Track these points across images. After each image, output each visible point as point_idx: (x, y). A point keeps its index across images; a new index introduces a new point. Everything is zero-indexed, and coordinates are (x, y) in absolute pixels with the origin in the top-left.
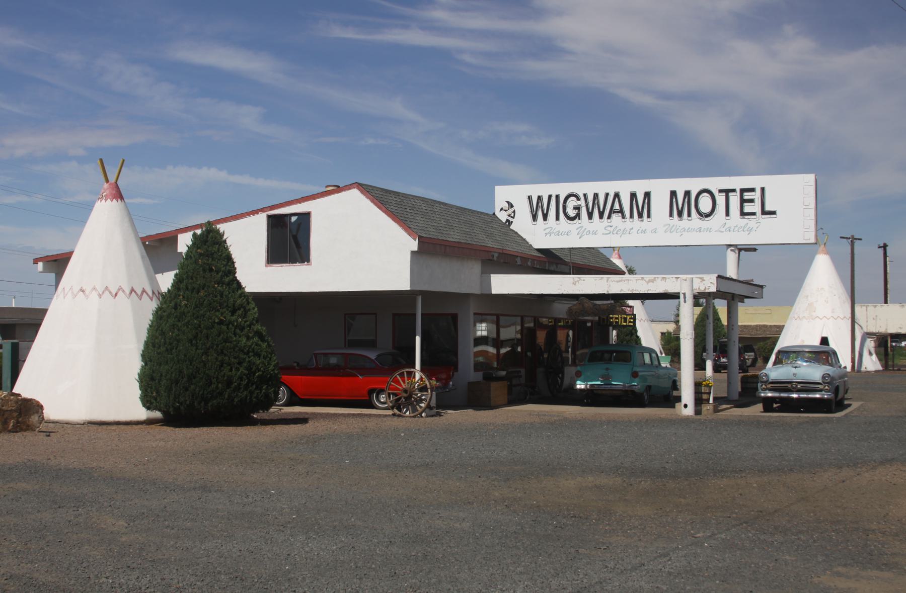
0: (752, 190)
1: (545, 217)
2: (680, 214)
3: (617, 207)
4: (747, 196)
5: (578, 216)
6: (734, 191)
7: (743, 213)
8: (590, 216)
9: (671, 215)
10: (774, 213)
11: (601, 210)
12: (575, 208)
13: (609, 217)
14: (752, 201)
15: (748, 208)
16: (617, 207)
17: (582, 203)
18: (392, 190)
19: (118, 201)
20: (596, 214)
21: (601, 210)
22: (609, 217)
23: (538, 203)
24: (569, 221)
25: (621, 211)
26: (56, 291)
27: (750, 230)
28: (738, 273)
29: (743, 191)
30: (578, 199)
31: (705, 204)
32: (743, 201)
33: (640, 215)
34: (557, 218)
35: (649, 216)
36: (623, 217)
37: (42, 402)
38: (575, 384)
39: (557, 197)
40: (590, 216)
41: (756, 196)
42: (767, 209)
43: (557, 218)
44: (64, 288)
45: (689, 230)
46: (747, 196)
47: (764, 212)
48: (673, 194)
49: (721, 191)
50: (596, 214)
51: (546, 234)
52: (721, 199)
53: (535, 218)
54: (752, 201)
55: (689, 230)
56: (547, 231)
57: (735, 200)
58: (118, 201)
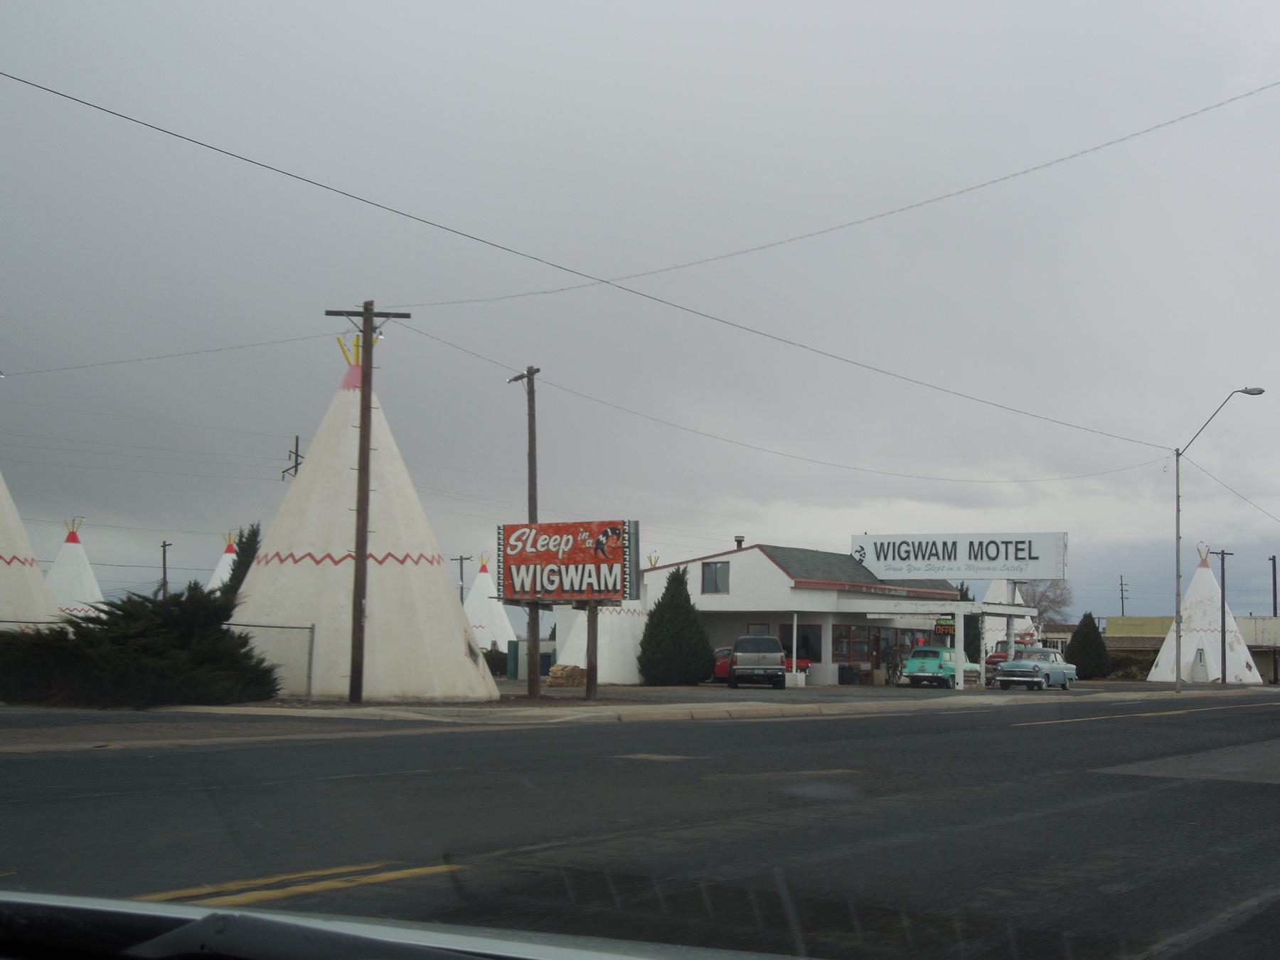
0: (1023, 542)
1: (886, 558)
2: (976, 558)
3: (934, 551)
4: (1020, 546)
5: (908, 557)
6: (1011, 542)
7: (1017, 558)
8: (916, 558)
9: (970, 558)
10: (1036, 558)
12: (906, 552)
13: (929, 559)
14: (1022, 550)
15: (1021, 554)
16: (934, 551)
17: (911, 548)
22: (929, 559)
25: (937, 555)
27: (1021, 570)
29: (1017, 543)
30: (908, 545)
31: (992, 551)
32: (1017, 550)
33: (949, 558)
34: (894, 559)
35: (955, 558)
36: (938, 559)
39: (894, 544)
40: (916, 558)
41: (1025, 546)
42: (1033, 555)
43: (894, 559)
45: (982, 569)
46: (1020, 546)
47: (1031, 558)
49: (1003, 542)
52: (1002, 547)
53: (878, 558)
54: (1022, 550)
55: (982, 569)
57: (1012, 548)
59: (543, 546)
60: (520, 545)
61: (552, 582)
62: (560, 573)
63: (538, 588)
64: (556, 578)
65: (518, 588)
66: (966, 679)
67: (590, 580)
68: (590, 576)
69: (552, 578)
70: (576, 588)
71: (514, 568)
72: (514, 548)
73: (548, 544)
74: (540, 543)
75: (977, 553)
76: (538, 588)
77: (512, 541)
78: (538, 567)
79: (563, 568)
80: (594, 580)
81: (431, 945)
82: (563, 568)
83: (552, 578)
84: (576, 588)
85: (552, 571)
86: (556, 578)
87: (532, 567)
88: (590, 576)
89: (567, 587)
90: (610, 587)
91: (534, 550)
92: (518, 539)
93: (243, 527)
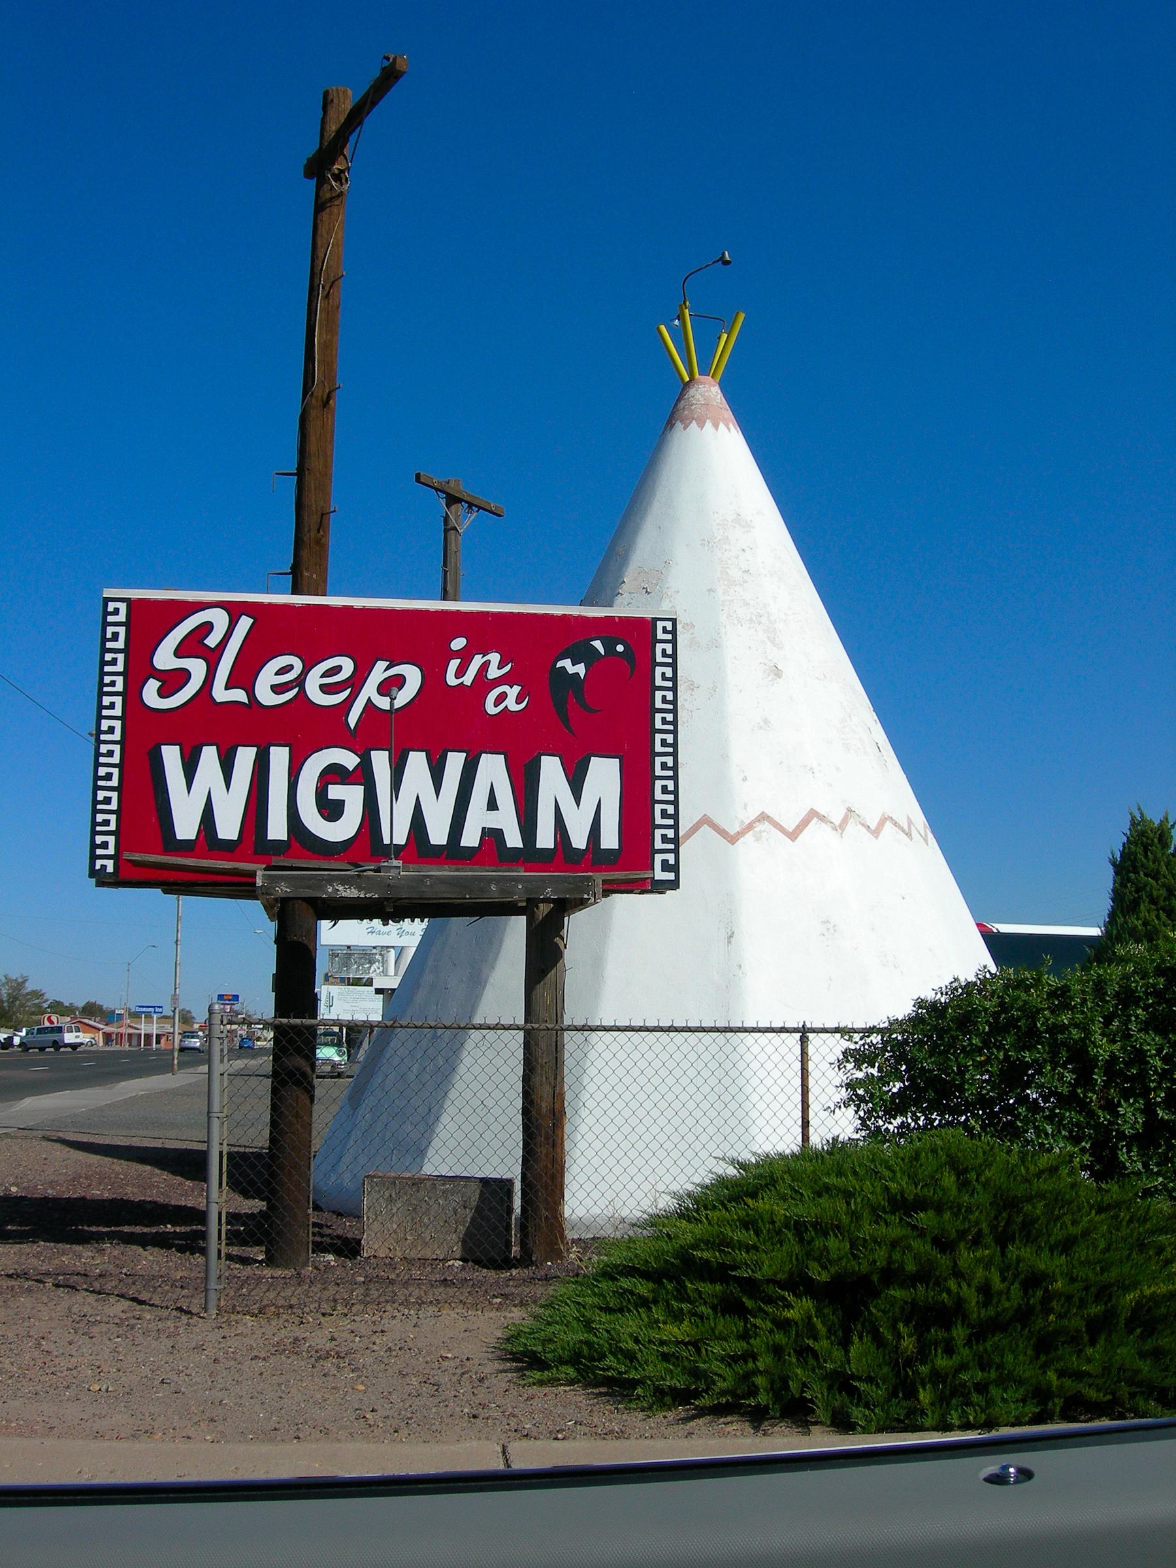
56: (370, 930)
59: (277, 689)
60: (197, 667)
61: (331, 810)
62: (363, 776)
63: (277, 829)
64: (351, 796)
65: (186, 827)
66: (250, 880)
67: (493, 820)
68: (492, 805)
69: (335, 792)
70: (438, 835)
71: (171, 756)
72: (179, 678)
73: (300, 681)
74: (267, 677)
75: (926, 835)
76: (277, 829)
77: (165, 658)
78: (279, 757)
79: (380, 761)
80: (507, 821)
81: (88, 869)
82: (380, 761)
83: (335, 792)
84: (438, 835)
85: (333, 774)
86: (351, 796)
87: (245, 757)
88: (492, 805)
89: (396, 830)
90: (579, 841)
91: (239, 695)
92: (192, 646)
93: (837, 1082)
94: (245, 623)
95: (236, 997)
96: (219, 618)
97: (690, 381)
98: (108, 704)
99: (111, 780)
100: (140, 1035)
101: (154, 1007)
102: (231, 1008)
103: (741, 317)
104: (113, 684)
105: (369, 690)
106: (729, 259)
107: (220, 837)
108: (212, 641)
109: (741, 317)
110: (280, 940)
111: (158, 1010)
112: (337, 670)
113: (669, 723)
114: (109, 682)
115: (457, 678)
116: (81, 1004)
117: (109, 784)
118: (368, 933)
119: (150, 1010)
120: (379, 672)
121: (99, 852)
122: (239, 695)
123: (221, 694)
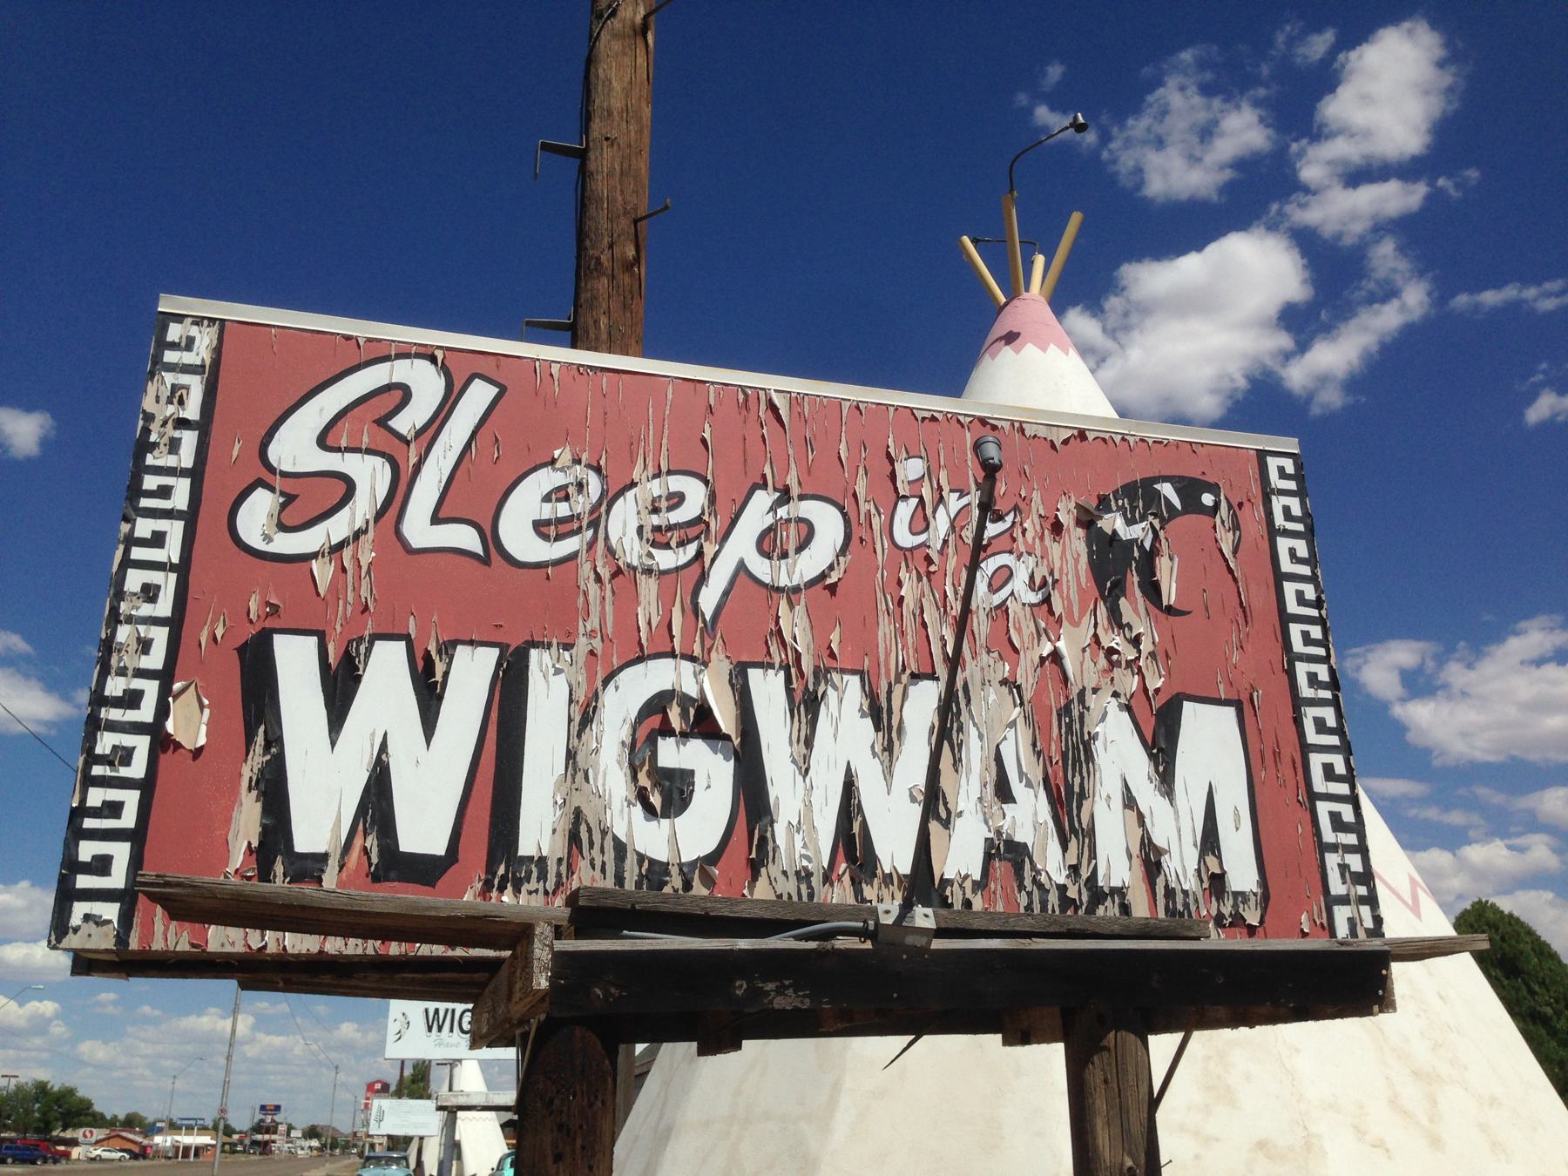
1: (440, 1029)
11: (440, 1023)
18: (919, 1041)
19: (1067, 354)
20: (435, 1028)
21: (440, 1023)
23: (434, 1017)
24: (461, 1034)
26: (1128, 848)
28: (506, 1089)
34: (451, 1030)
37: (648, 823)
38: (37, 1118)
43: (451, 1030)
44: (1237, 829)
48: (427, 1011)
50: (435, 1028)
51: (436, 1045)
53: (430, 1029)
56: (437, 1042)
58: (1067, 354)
83: (670, 754)
91: (465, 537)
94: (479, 396)
95: (277, 1108)
96: (427, 385)
97: (1006, 304)
98: (148, 536)
99: (138, 707)
100: (179, 1147)
101: (195, 1119)
102: (272, 1119)
103: (1076, 218)
104: (165, 492)
105: (742, 545)
106: (1083, 121)
107: (401, 850)
108: (405, 423)
109: (1076, 218)
110: (614, 1146)
111: (199, 1122)
112: (677, 499)
113: (1315, 643)
114: (154, 488)
115: (913, 534)
116: (122, 1116)
117: (131, 716)
118: (436, 1045)
119: (191, 1122)
120: (758, 513)
121: (84, 881)
122: (465, 537)
123: (419, 529)
